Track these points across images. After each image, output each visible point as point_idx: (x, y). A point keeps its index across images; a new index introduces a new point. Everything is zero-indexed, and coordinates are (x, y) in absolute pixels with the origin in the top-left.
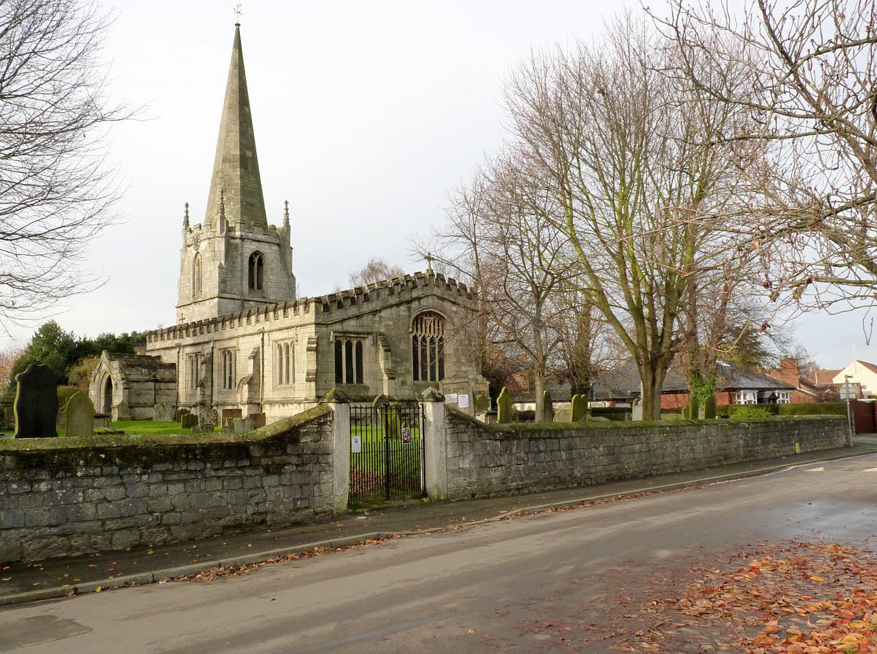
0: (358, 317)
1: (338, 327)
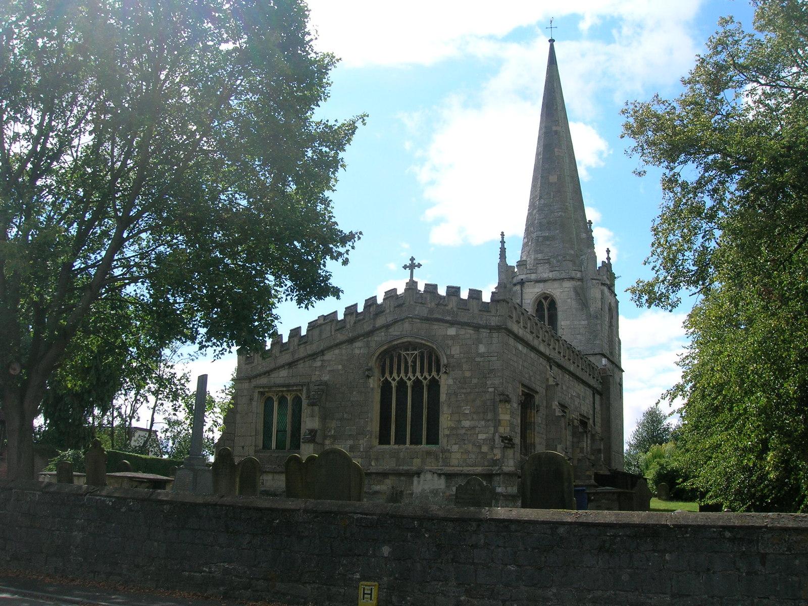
0: (290, 365)
1: (263, 381)
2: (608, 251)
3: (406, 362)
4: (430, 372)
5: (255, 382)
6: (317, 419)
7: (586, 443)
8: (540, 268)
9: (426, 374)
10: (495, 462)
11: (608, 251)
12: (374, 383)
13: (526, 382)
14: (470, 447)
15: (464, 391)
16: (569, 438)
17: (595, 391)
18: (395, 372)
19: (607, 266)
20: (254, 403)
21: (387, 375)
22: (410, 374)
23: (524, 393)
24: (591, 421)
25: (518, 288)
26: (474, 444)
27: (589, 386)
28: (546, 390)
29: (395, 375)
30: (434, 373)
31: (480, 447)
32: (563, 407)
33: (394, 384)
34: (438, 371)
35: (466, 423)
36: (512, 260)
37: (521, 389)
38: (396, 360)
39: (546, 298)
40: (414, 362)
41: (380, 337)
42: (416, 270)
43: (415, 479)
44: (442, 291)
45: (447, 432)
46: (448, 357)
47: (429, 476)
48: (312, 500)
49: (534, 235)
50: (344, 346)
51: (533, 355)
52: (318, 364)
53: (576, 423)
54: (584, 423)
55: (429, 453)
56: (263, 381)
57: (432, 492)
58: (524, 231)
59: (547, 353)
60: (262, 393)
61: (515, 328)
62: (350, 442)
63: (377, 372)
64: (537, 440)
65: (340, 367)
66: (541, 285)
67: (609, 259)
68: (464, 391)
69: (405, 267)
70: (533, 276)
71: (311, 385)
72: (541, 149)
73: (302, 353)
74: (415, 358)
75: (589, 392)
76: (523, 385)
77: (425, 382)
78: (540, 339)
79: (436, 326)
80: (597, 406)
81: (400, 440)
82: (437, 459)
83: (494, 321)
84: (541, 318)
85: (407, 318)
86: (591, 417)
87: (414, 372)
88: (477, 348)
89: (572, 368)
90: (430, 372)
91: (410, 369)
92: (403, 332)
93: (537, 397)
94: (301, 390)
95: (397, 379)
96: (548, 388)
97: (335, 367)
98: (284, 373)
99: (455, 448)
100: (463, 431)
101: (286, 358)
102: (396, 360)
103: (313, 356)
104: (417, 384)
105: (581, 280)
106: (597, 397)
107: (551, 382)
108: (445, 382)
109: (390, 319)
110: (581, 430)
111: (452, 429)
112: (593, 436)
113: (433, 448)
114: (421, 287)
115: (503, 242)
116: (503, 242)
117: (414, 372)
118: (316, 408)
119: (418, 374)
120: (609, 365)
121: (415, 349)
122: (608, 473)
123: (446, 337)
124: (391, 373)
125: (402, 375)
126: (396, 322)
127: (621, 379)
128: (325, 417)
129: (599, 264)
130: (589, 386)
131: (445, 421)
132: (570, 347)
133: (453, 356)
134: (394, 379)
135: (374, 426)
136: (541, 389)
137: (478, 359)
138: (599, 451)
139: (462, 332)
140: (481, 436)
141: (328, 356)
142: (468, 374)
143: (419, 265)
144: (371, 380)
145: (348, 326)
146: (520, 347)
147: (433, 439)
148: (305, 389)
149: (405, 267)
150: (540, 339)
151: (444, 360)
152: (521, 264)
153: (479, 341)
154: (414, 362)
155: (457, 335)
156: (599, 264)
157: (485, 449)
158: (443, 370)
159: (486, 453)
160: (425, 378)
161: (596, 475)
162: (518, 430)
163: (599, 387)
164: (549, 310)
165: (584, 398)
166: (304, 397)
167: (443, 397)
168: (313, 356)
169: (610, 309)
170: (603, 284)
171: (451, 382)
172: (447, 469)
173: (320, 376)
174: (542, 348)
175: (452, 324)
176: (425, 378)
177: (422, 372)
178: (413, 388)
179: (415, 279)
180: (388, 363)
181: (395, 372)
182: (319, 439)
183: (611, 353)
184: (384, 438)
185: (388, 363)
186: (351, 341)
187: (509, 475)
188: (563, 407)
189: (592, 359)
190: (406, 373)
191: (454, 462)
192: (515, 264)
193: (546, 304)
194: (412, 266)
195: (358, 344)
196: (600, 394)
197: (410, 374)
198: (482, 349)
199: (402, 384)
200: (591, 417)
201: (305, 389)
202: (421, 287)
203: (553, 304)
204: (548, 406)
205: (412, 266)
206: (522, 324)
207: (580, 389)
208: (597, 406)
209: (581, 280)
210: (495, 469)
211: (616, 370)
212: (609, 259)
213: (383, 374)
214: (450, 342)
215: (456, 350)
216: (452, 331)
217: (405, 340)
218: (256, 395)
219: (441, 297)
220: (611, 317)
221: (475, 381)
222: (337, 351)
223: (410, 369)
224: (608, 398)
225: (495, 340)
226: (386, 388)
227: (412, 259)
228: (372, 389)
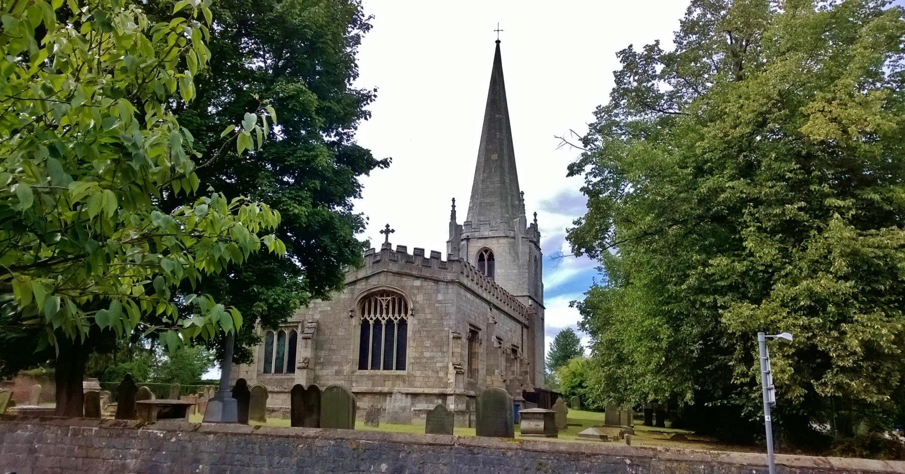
2: (535, 214)
3: (381, 306)
4: (400, 313)
6: (309, 350)
7: (516, 367)
8: (482, 228)
9: (396, 315)
11: (535, 214)
12: (356, 322)
13: (473, 322)
14: (430, 373)
16: (504, 363)
17: (524, 326)
19: (534, 226)
21: (366, 315)
22: (384, 315)
23: (471, 331)
24: (520, 349)
25: (464, 242)
26: (433, 371)
27: (519, 322)
29: (372, 315)
30: (403, 315)
31: (437, 372)
32: (499, 339)
33: (371, 322)
34: (406, 313)
36: (461, 220)
37: (469, 327)
38: (373, 304)
39: (486, 251)
40: (388, 306)
41: (361, 287)
42: (390, 235)
43: (388, 398)
44: (410, 252)
45: (412, 361)
46: (414, 302)
47: (399, 396)
48: (869, 400)
49: (478, 201)
51: (478, 300)
53: (509, 351)
54: (514, 351)
55: (398, 376)
57: (401, 408)
58: (469, 201)
59: (488, 299)
61: (466, 281)
62: (336, 368)
63: (358, 313)
64: (480, 367)
65: (329, 308)
66: (483, 241)
67: (535, 220)
69: (382, 232)
70: (477, 234)
71: (306, 322)
72: (483, 147)
74: (388, 302)
75: (519, 327)
76: (470, 325)
77: (395, 322)
80: (525, 337)
81: (375, 366)
82: (404, 382)
83: (449, 277)
84: (482, 267)
86: (520, 346)
87: (387, 313)
88: (437, 296)
89: (506, 309)
90: (400, 313)
91: (384, 311)
93: (480, 333)
94: (297, 327)
95: (374, 318)
96: (488, 325)
99: (418, 373)
100: (425, 360)
102: (373, 304)
104: (390, 322)
105: (513, 238)
106: (525, 330)
107: (491, 321)
108: (411, 322)
109: (369, 273)
110: (512, 357)
111: (415, 358)
112: (521, 360)
114: (394, 248)
115: (454, 206)
116: (454, 206)
117: (387, 313)
118: (309, 341)
119: (390, 315)
120: (534, 305)
121: (388, 296)
122: (533, 391)
123: (412, 287)
124: (369, 314)
125: (378, 315)
127: (543, 315)
129: (528, 225)
130: (519, 322)
131: (411, 353)
132: (505, 293)
133: (418, 302)
135: (355, 355)
136: (483, 327)
137: (437, 305)
138: (526, 373)
139: (425, 284)
140: (438, 365)
142: (429, 316)
143: (393, 231)
144: (353, 320)
147: (401, 366)
148: (300, 326)
149: (382, 232)
150: (475, 282)
151: (411, 306)
152: (467, 224)
153: (438, 291)
154: (388, 306)
155: (422, 286)
156: (528, 225)
158: (410, 312)
160: (396, 319)
161: (524, 392)
162: (466, 359)
163: (526, 322)
164: (489, 260)
165: (515, 332)
166: (299, 331)
167: (409, 333)
169: (535, 260)
170: (531, 241)
171: (416, 322)
172: (412, 390)
173: (313, 315)
174: (485, 295)
175: (418, 278)
176: (396, 318)
177: (393, 313)
178: (386, 325)
179: (389, 241)
180: (367, 306)
183: (536, 295)
184: (363, 365)
185: (367, 306)
188: (499, 339)
189: (520, 300)
190: (381, 314)
192: (462, 224)
193: (486, 257)
194: (387, 231)
196: (527, 327)
197: (384, 315)
199: (377, 322)
200: (520, 346)
201: (300, 326)
202: (394, 248)
203: (491, 257)
204: (489, 340)
205: (387, 231)
207: (512, 324)
208: (525, 337)
209: (513, 238)
211: (539, 308)
212: (535, 220)
213: (363, 314)
214: (416, 292)
215: (420, 298)
216: (417, 283)
219: (409, 256)
220: (536, 267)
221: (434, 322)
223: (384, 311)
224: (533, 332)
226: (365, 325)
227: (388, 226)
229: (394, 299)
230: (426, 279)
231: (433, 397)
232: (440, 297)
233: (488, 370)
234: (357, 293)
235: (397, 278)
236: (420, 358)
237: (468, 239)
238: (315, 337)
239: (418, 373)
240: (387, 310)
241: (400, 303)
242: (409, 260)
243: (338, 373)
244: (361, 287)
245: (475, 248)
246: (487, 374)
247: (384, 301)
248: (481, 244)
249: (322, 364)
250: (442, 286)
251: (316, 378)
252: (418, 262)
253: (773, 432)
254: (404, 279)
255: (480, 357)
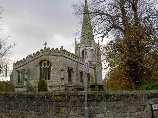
0: (23, 66)
1: (18, 69)
3: (44, 64)
5: (16, 70)
10: (60, 83)
12: (38, 68)
14: (56, 80)
15: (55, 69)
18: (47, 65)
20: (16, 74)
24: (91, 75)
28: (76, 68)
30: (50, 66)
35: (55, 76)
41: (39, 59)
50: (33, 61)
51: (72, 61)
52: (28, 65)
56: (18, 69)
60: (18, 72)
63: (39, 66)
64: (74, 79)
68: (55, 69)
69: (44, 44)
70: (81, 46)
73: (25, 63)
78: (74, 58)
79: (49, 56)
83: (60, 54)
85: (44, 55)
87: (46, 66)
92: (44, 57)
95: (49, 67)
97: (31, 66)
98: (22, 67)
99: (53, 81)
101: (22, 64)
102: (42, 63)
103: (27, 64)
106: (93, 70)
108: (51, 67)
113: (49, 81)
114: (47, 48)
115: (76, 40)
116: (76, 40)
117: (46, 66)
118: (27, 74)
126: (42, 56)
128: (29, 76)
131: (51, 76)
134: (42, 67)
139: (54, 57)
141: (30, 63)
143: (47, 44)
144: (38, 68)
145: (33, 57)
146: (68, 60)
147: (49, 79)
149: (44, 44)
150: (74, 58)
155: (53, 58)
157: (59, 81)
159: (59, 82)
168: (27, 64)
171: (52, 67)
174: (75, 60)
175: (53, 55)
176: (48, 66)
177: (47, 66)
179: (46, 47)
180: (41, 64)
181: (41, 66)
182: (28, 80)
186: (34, 60)
187: (63, 86)
191: (53, 84)
194: (45, 44)
195: (35, 61)
198: (58, 60)
202: (47, 48)
205: (45, 44)
206: (68, 55)
210: (60, 85)
213: (40, 66)
215: (53, 61)
216: (52, 57)
217: (44, 59)
218: (17, 72)
221: (57, 67)
222: (31, 62)
223: (45, 65)
225: (61, 58)
227: (45, 43)
228: (38, 70)
229: (47, 62)
230: (55, 55)
231: (57, 87)
232: (58, 60)
233: (77, 80)
234: (38, 61)
235: (48, 56)
236: (53, 77)
237: (79, 48)
238: (28, 73)
239: (53, 81)
240: (46, 65)
241: (49, 63)
242: (50, 51)
243: (34, 82)
244: (39, 59)
245: (81, 49)
246: (77, 81)
247: (45, 62)
248: (83, 48)
249: (31, 80)
250: (59, 57)
251: (29, 83)
252: (57, 51)
253: (46, 73)
254: (50, 56)
255: (73, 76)
